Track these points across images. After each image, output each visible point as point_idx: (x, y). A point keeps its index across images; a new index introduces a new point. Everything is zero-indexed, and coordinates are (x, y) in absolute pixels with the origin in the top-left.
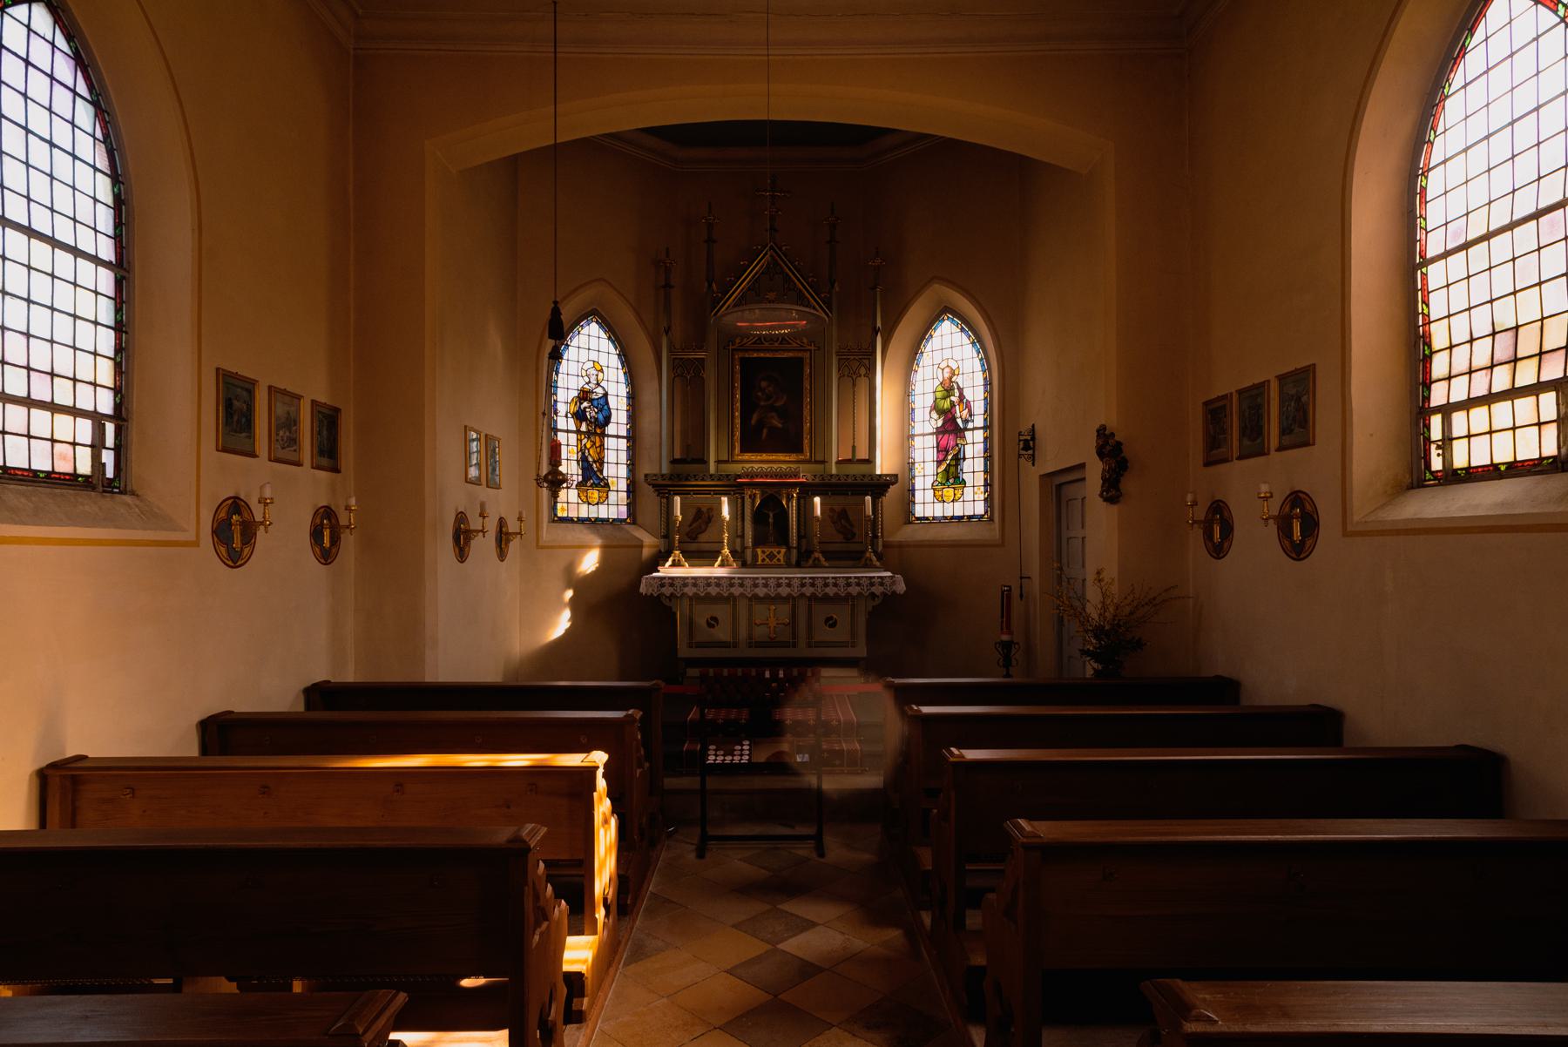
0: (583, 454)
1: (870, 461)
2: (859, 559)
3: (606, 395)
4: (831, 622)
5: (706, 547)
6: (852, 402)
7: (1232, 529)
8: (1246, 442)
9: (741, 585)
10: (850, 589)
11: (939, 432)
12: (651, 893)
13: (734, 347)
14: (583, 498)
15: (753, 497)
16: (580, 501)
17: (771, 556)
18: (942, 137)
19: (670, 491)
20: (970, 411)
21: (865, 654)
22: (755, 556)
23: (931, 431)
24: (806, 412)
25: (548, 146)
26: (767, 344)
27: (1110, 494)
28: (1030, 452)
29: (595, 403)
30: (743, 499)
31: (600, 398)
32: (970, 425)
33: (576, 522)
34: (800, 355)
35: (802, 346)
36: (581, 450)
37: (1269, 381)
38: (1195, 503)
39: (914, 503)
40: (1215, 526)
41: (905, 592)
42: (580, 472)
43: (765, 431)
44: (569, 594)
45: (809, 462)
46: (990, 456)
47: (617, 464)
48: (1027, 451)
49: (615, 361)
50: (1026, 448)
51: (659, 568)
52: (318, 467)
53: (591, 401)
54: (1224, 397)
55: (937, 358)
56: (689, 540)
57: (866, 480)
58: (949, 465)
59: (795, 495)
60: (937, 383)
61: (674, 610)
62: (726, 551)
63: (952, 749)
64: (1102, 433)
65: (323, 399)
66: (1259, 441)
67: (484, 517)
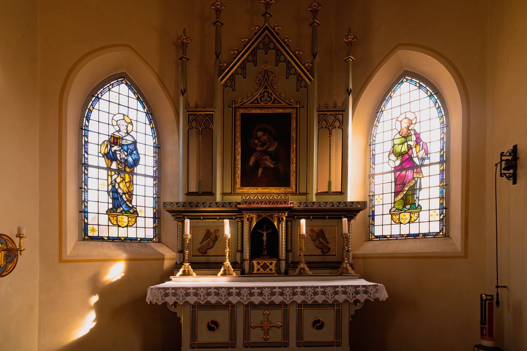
0: (114, 186)
1: (343, 192)
2: (337, 268)
3: (135, 143)
5: (212, 259)
6: (329, 151)
9: (239, 294)
10: (337, 297)
13: (236, 106)
14: (113, 221)
15: (250, 220)
16: (110, 224)
17: (265, 267)
19: (184, 216)
22: (252, 267)
23: (390, 169)
24: (293, 156)
26: (262, 104)
31: (130, 144)
32: (426, 162)
33: (106, 241)
35: (290, 105)
36: (111, 183)
39: (374, 225)
42: (111, 201)
43: (260, 171)
44: (95, 299)
45: (292, 194)
46: (446, 185)
47: (145, 196)
48: (508, 170)
49: (142, 117)
51: (171, 277)
53: (122, 146)
55: (396, 113)
56: (200, 254)
57: (341, 206)
58: (406, 195)
59: (284, 218)
61: (178, 315)
62: (228, 263)
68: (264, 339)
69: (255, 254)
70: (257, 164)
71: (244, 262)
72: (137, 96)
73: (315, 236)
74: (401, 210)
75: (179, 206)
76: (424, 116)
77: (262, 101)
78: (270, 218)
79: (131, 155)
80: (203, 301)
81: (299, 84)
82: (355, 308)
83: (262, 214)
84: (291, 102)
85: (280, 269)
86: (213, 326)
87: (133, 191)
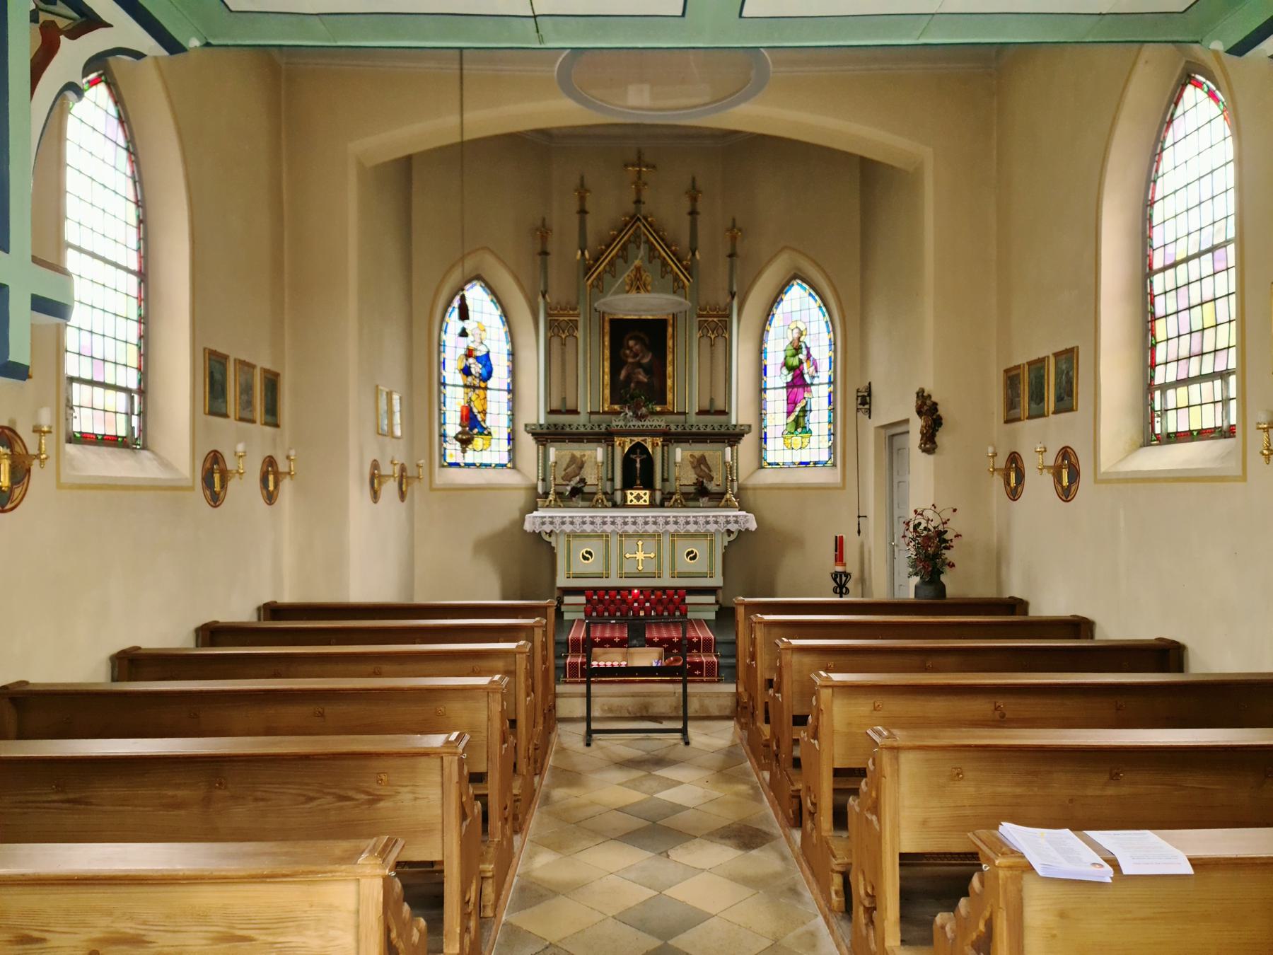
3: (487, 355)
7: (1024, 476)
8: (1033, 406)
11: (789, 386)
12: (551, 765)
19: (547, 439)
20: (816, 368)
22: (624, 498)
28: (867, 406)
30: (613, 446)
32: (816, 381)
33: (463, 467)
37: (1048, 357)
38: (995, 455)
40: (1064, 470)
41: (756, 529)
50: (863, 403)
52: (266, 424)
54: (1018, 367)
60: (788, 342)
61: (553, 544)
63: (783, 639)
66: (1041, 405)
70: (629, 378)
73: (695, 463)
74: (793, 434)
76: (813, 329)
78: (643, 443)
81: (676, 284)
82: (727, 539)
85: (655, 500)
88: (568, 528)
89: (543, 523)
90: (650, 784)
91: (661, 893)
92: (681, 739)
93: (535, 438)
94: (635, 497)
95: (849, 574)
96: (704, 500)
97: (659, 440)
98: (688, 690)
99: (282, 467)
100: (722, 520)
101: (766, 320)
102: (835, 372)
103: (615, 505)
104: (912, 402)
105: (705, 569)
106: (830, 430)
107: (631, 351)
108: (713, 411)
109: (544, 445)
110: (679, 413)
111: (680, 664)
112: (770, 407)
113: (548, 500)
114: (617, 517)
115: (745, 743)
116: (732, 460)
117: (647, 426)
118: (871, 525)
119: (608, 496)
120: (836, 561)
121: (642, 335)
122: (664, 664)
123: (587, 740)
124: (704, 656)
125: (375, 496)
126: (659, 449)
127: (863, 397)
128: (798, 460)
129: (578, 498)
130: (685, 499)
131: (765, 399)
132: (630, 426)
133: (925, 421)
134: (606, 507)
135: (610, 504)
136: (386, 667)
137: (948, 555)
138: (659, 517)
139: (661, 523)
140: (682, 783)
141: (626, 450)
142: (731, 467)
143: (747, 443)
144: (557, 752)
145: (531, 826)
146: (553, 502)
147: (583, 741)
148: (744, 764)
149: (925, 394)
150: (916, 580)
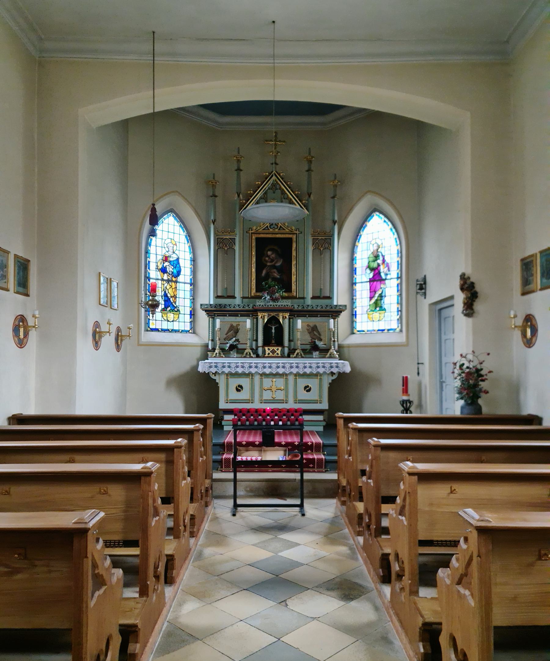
0: (165, 292)
3: (178, 259)
4: (308, 389)
8: (545, 280)
11: (371, 281)
13: (253, 232)
14: (164, 317)
15: (263, 318)
16: (163, 320)
17: (273, 352)
18: (373, 110)
19: (215, 314)
21: (327, 408)
22: (264, 352)
25: (149, 114)
26: (271, 230)
27: (467, 312)
28: (423, 291)
29: (172, 263)
30: (257, 319)
32: (388, 277)
34: (290, 236)
35: (291, 231)
36: (164, 290)
38: (515, 316)
41: (350, 372)
50: (421, 288)
52: (18, 293)
53: (170, 262)
57: (328, 308)
58: (377, 300)
60: (370, 253)
61: (217, 381)
64: (464, 278)
65: (20, 254)
67: (110, 324)
68: (272, 397)
69: (267, 342)
70: (268, 276)
71: (258, 348)
72: (179, 224)
73: (310, 330)
74: (373, 311)
75: (212, 307)
77: (271, 228)
78: (277, 317)
79: (175, 268)
80: (233, 371)
82: (331, 378)
83: (272, 314)
84: (292, 229)
85: (284, 353)
86: (239, 388)
87: (177, 295)
88: (227, 370)
89: (211, 367)
90: (276, 545)
91: (279, 639)
92: (300, 511)
93: (207, 314)
94: (271, 352)
95: (412, 401)
96: (315, 354)
97: (287, 315)
98: (304, 478)
99: (31, 322)
100: (327, 366)
101: (356, 239)
102: (401, 271)
103: (258, 356)
104: (457, 282)
105: (316, 398)
106: (398, 308)
107: (269, 258)
108: (322, 296)
109: (213, 318)
110: (300, 298)
111: (298, 459)
112: (358, 295)
113: (215, 353)
114: (259, 363)
115: (344, 515)
116: (334, 327)
117: (279, 306)
118: (426, 369)
119: (253, 351)
120: (403, 393)
121: (276, 248)
122: (287, 459)
123: (234, 512)
124: (316, 454)
125: (97, 344)
126: (287, 321)
127: (421, 285)
128: (376, 328)
129: (234, 351)
130: (303, 353)
131: (356, 289)
132: (268, 306)
133: (466, 294)
134: (252, 357)
135: (255, 356)
136: (77, 457)
137: (483, 385)
138: (286, 363)
139: (288, 367)
140: (299, 545)
141: (266, 321)
142: (334, 333)
143: (344, 317)
144: (211, 520)
145: (184, 578)
146: (218, 355)
147: (231, 512)
148: (345, 530)
149: (466, 277)
150: (462, 402)
